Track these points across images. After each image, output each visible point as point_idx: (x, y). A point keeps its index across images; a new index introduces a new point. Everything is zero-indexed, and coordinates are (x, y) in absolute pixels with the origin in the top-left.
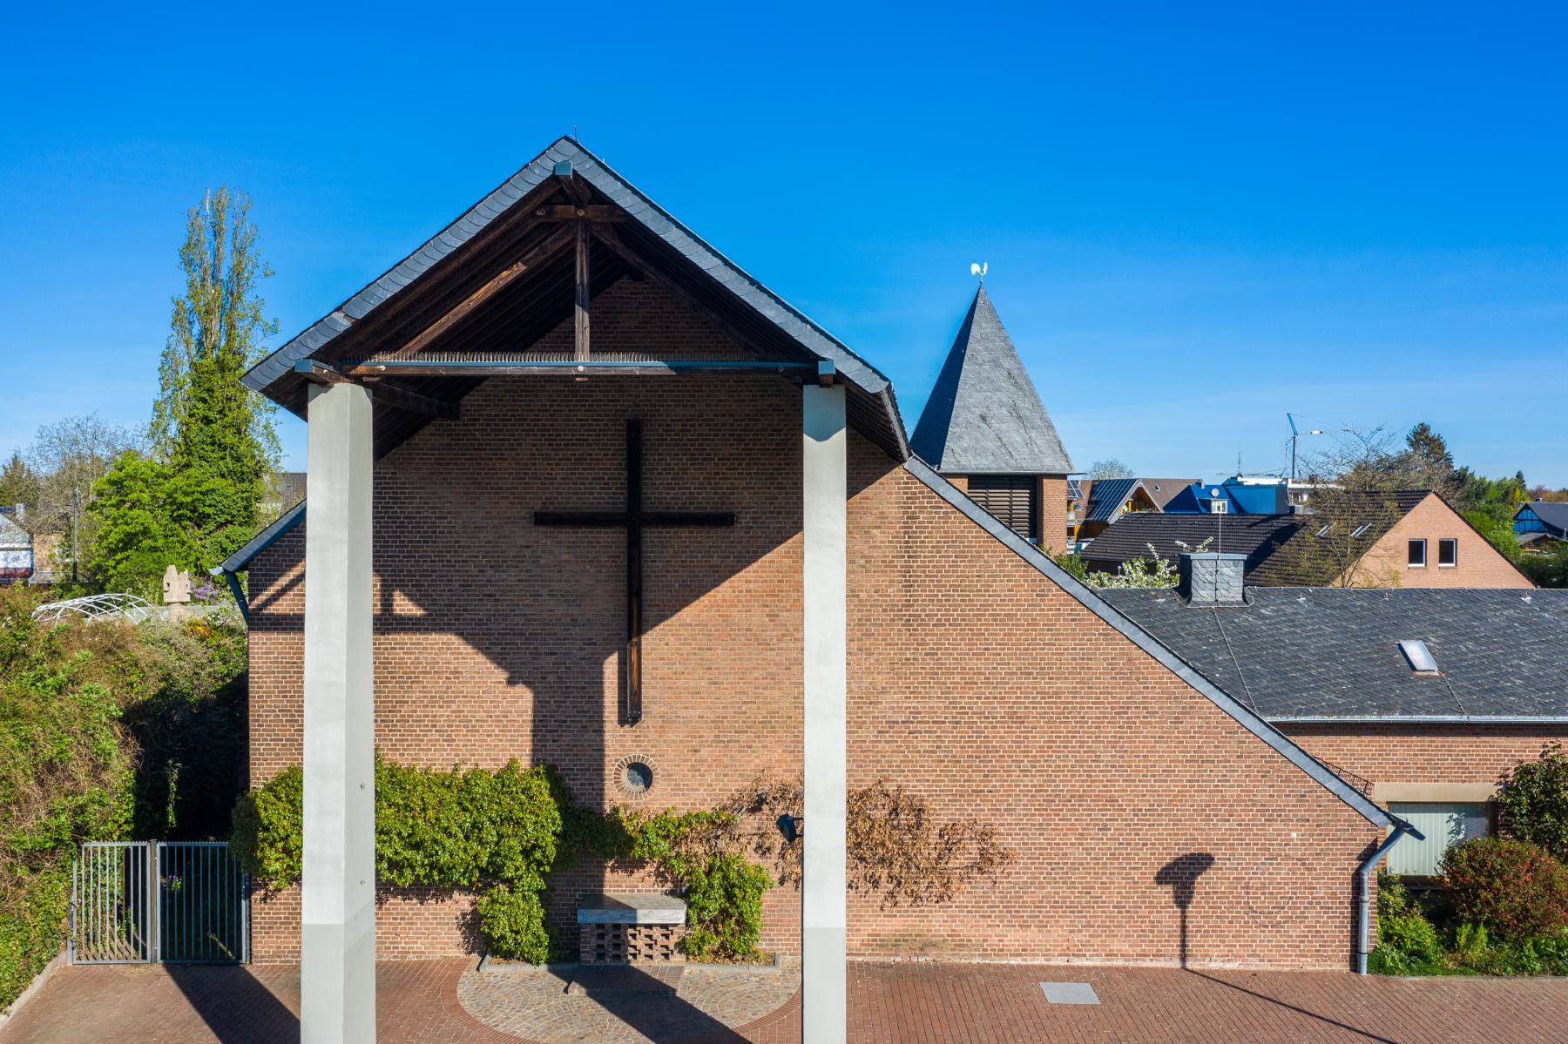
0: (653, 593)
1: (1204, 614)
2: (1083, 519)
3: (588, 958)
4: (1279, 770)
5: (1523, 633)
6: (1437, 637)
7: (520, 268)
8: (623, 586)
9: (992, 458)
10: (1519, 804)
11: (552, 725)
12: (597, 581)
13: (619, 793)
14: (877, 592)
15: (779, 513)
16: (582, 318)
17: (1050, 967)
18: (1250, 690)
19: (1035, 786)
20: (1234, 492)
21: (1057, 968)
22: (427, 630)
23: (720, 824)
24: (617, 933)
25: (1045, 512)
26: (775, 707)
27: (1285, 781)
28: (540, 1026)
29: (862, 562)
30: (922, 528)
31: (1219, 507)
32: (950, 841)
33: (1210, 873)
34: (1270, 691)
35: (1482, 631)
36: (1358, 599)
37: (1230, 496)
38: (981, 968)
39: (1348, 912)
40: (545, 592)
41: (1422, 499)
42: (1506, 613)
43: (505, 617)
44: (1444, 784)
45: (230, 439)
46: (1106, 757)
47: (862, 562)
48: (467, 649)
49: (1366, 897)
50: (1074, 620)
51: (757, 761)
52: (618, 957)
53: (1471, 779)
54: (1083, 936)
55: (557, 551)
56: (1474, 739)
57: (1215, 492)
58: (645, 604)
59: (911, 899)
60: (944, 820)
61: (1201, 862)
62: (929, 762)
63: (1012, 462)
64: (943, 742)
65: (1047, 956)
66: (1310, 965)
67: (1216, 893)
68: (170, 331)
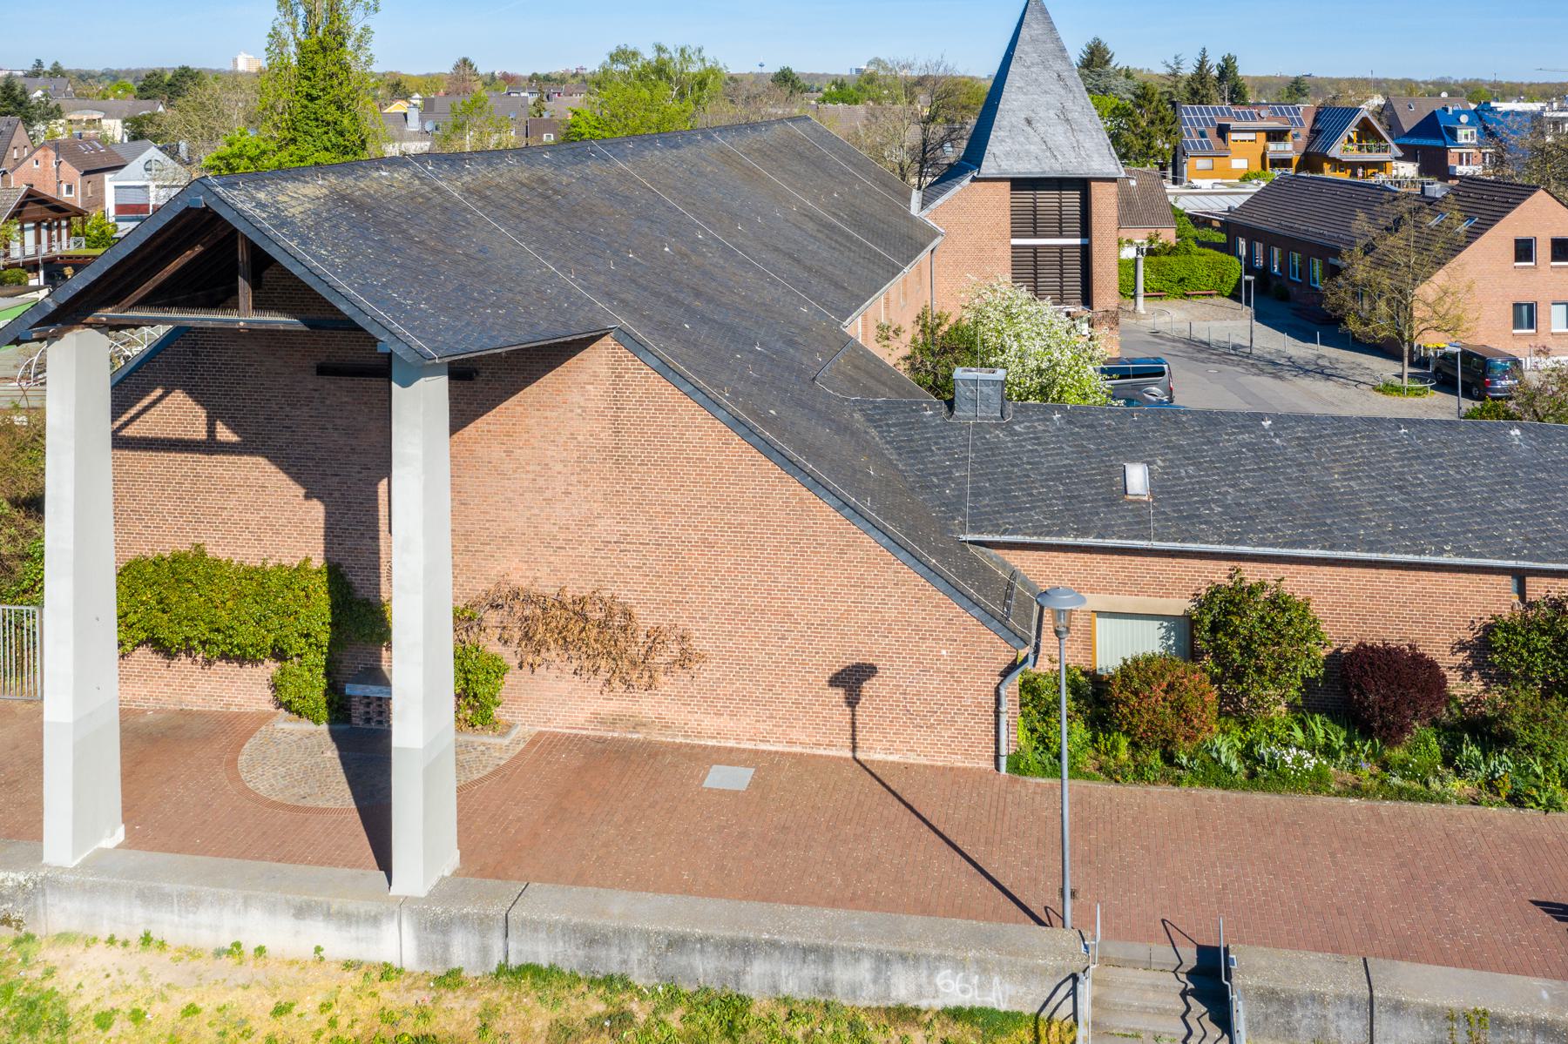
2: (1303, 151)
3: (357, 721)
4: (930, 597)
6: (1163, 461)
7: (199, 249)
9: (1035, 162)
11: (337, 532)
12: (371, 419)
14: (591, 435)
15: (512, 370)
16: (244, 287)
18: (970, 507)
19: (724, 600)
22: (240, 453)
24: (379, 703)
25: (1093, 215)
26: (512, 525)
27: (935, 607)
29: (579, 411)
30: (627, 385)
34: (988, 509)
36: (1110, 418)
40: (330, 426)
41: (1530, 195)
43: (300, 445)
44: (1142, 598)
45: (332, 114)
46: (783, 579)
47: (579, 411)
50: (754, 465)
51: (499, 568)
53: (1168, 595)
54: (770, 724)
55: (338, 394)
56: (1170, 560)
57: (1464, 119)
59: (624, 687)
60: (651, 623)
62: (637, 577)
64: (648, 560)
66: (959, 762)
67: (878, 696)
68: (276, 14)
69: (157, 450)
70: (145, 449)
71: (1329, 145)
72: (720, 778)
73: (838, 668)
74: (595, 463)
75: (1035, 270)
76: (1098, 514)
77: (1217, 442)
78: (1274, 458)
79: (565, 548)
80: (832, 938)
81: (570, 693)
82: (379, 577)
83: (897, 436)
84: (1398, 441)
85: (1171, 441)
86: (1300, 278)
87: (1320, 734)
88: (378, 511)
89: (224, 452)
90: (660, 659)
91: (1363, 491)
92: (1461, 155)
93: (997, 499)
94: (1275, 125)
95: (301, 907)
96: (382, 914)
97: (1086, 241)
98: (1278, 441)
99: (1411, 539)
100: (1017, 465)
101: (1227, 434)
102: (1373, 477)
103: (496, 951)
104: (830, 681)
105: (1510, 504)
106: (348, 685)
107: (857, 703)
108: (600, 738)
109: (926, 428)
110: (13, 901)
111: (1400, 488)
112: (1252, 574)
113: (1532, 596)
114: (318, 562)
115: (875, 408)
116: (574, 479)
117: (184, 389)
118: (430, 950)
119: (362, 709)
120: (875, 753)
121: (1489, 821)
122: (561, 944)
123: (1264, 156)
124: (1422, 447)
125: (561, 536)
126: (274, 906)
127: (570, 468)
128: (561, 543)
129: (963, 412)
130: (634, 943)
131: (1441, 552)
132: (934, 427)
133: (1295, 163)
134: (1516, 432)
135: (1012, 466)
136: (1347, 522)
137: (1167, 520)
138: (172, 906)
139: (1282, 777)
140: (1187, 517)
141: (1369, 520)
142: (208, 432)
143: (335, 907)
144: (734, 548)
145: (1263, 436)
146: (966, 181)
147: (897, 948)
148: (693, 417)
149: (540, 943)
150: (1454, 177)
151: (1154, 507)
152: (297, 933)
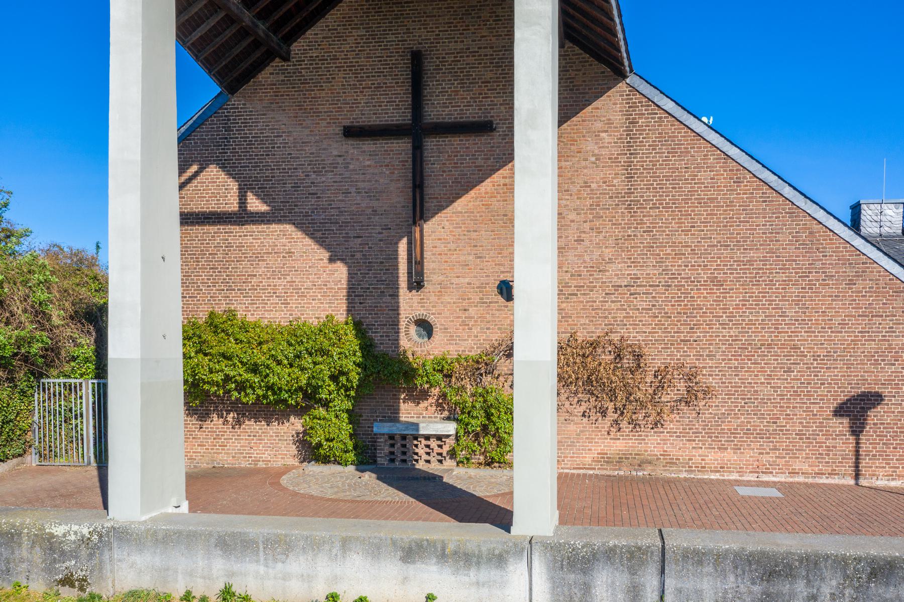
11: (359, 291)
12: (391, 181)
14: (605, 182)
19: (731, 336)
22: (269, 222)
29: (593, 159)
32: (662, 378)
40: (353, 190)
46: (790, 313)
47: (593, 159)
50: (765, 201)
52: (404, 461)
64: (657, 301)
73: (842, 398)
74: (608, 209)
79: (576, 295)
81: (579, 435)
82: (398, 332)
88: (398, 269)
89: (254, 222)
90: (668, 397)
95: (410, 549)
96: (507, 552)
103: (649, 590)
104: (835, 411)
106: (375, 424)
107: (862, 431)
110: (76, 557)
114: (341, 316)
116: (587, 226)
117: (217, 164)
118: (567, 593)
122: (732, 578)
125: (574, 283)
126: (379, 548)
127: (583, 216)
128: (573, 290)
130: (827, 574)
138: (257, 554)
142: (239, 203)
144: (742, 285)
149: (705, 579)
152: (406, 579)
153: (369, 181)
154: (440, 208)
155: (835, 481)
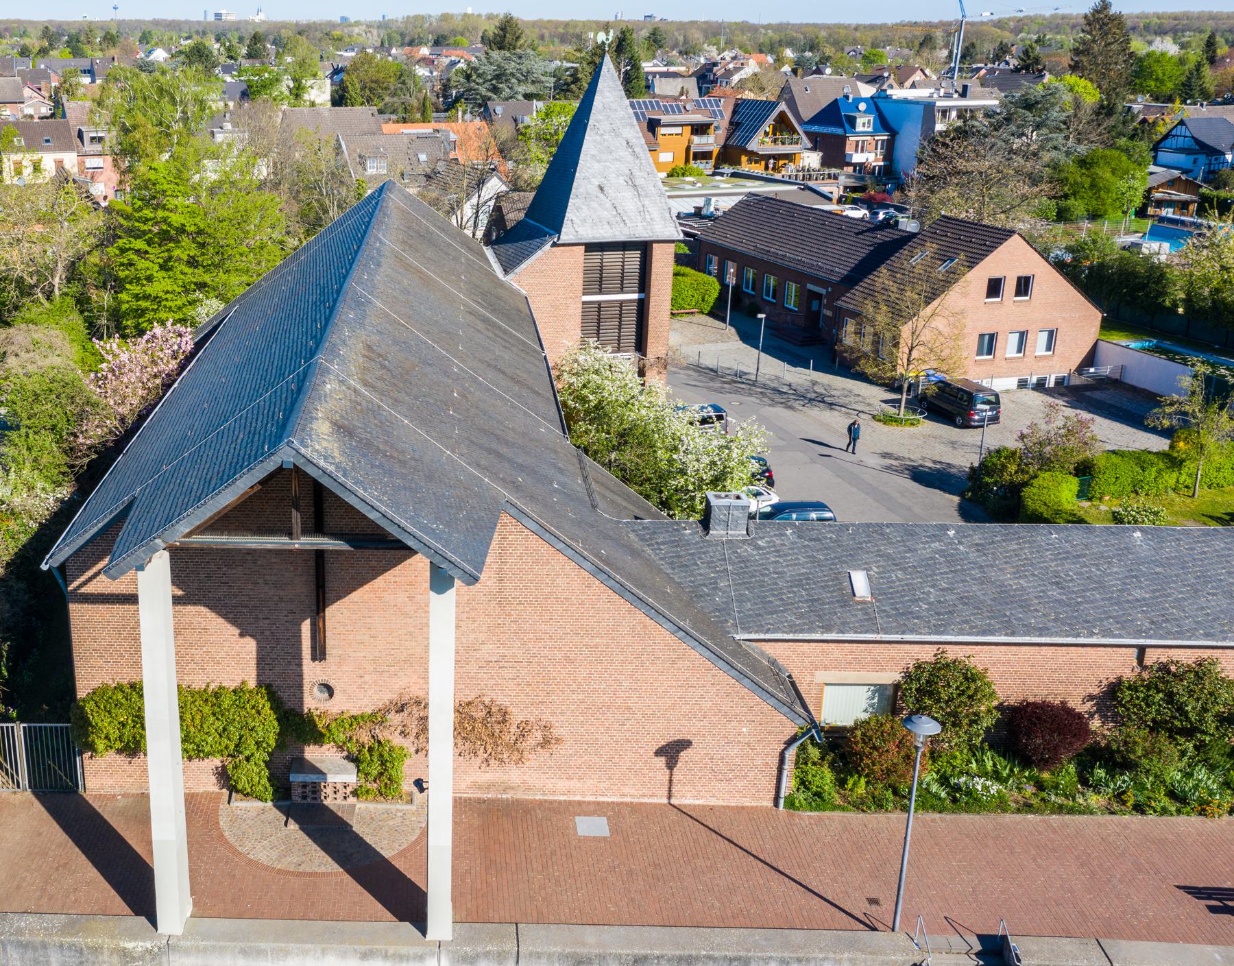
0: (331, 583)
1: (717, 545)
2: (722, 144)
3: (296, 798)
5: (940, 564)
6: (878, 567)
8: (313, 578)
10: (911, 689)
11: (268, 660)
13: (312, 702)
17: (584, 802)
20: (881, 104)
21: (589, 803)
22: (185, 604)
23: (376, 718)
28: (274, 854)
30: (510, 545)
31: (864, 124)
32: (524, 731)
33: (689, 750)
34: (751, 612)
35: (911, 559)
37: (878, 109)
38: (541, 803)
39: (775, 773)
42: (932, 545)
46: (626, 683)
48: (211, 615)
49: (786, 767)
52: (315, 799)
53: (882, 670)
54: (607, 784)
57: (862, 106)
58: (327, 590)
61: (684, 744)
63: (626, 229)
65: (583, 795)
66: (748, 802)
69: (113, 603)
70: (103, 602)
71: (748, 139)
72: (591, 827)
73: (663, 743)
75: (598, 323)
76: (836, 613)
77: (916, 550)
78: (961, 563)
80: (749, 951)
83: (667, 553)
84: (1051, 544)
85: (881, 550)
86: (753, 289)
87: (989, 765)
91: (1029, 588)
92: (857, 142)
93: (756, 604)
94: (699, 118)
95: (366, 953)
97: (643, 296)
98: (961, 548)
99: (1069, 625)
100: (767, 575)
101: (922, 543)
102: (1036, 576)
105: (1138, 594)
108: (479, 799)
109: (689, 545)
111: (1057, 584)
112: (952, 653)
113: (1148, 661)
115: (644, 528)
116: (465, 616)
119: (300, 790)
120: (685, 798)
121: (1126, 827)
123: (688, 149)
124: (1071, 549)
129: (716, 532)
131: (1092, 634)
132: (695, 544)
133: (715, 155)
134: (1138, 534)
135: (763, 575)
136: (1020, 613)
137: (888, 616)
139: (977, 800)
140: (903, 614)
141: (1037, 610)
143: (391, 952)
145: (951, 544)
146: (547, 247)
147: (794, 955)
148: (563, 567)
150: (849, 164)
151: (877, 607)
153: (276, 575)
154: (339, 598)
155: (655, 800)
